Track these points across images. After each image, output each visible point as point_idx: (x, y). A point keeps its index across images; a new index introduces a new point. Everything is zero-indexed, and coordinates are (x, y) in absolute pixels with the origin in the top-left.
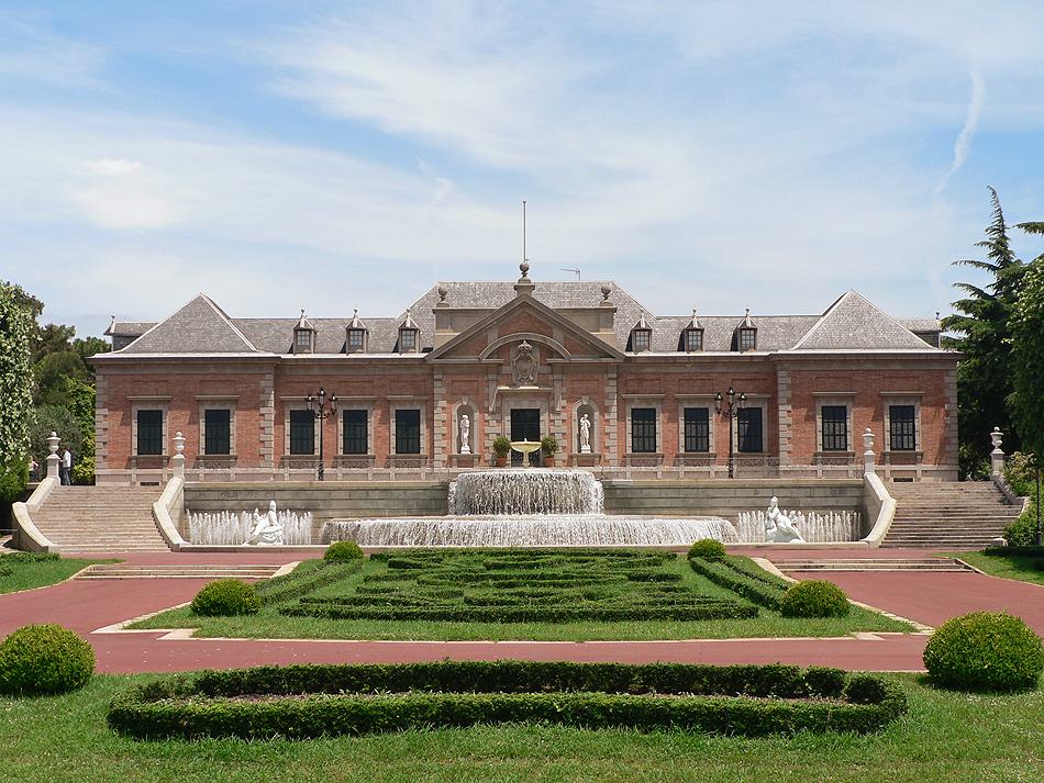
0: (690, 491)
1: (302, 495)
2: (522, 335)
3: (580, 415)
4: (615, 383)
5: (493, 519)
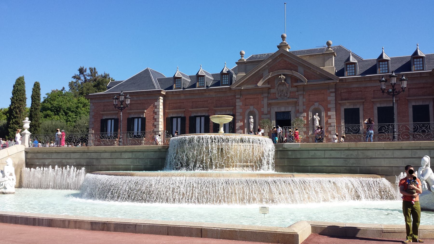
0: (351, 152)
1: (85, 156)
2: (280, 72)
3: (314, 114)
4: (333, 94)
5: (202, 175)
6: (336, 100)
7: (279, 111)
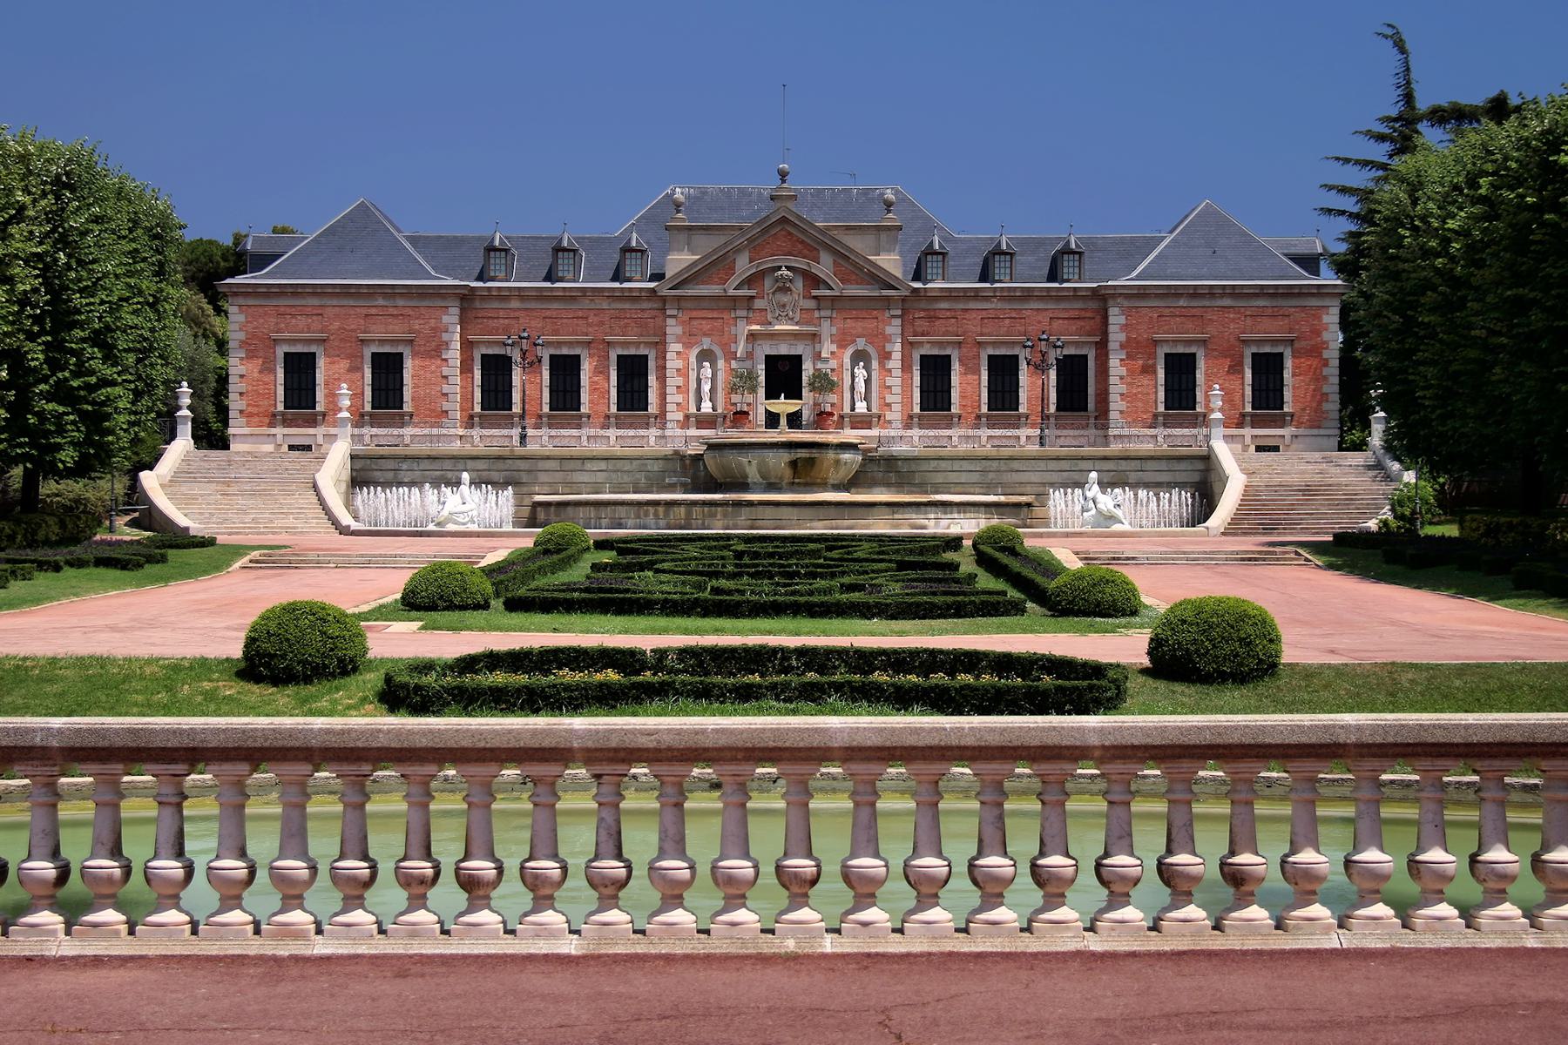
0: (989, 463)
4: (898, 322)
6: (902, 334)
7: (774, 352)
